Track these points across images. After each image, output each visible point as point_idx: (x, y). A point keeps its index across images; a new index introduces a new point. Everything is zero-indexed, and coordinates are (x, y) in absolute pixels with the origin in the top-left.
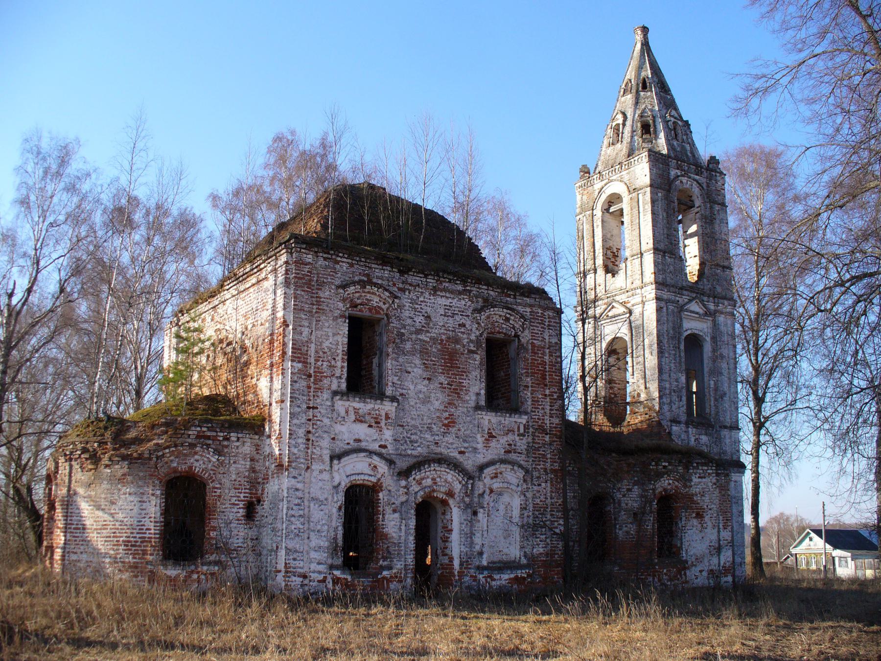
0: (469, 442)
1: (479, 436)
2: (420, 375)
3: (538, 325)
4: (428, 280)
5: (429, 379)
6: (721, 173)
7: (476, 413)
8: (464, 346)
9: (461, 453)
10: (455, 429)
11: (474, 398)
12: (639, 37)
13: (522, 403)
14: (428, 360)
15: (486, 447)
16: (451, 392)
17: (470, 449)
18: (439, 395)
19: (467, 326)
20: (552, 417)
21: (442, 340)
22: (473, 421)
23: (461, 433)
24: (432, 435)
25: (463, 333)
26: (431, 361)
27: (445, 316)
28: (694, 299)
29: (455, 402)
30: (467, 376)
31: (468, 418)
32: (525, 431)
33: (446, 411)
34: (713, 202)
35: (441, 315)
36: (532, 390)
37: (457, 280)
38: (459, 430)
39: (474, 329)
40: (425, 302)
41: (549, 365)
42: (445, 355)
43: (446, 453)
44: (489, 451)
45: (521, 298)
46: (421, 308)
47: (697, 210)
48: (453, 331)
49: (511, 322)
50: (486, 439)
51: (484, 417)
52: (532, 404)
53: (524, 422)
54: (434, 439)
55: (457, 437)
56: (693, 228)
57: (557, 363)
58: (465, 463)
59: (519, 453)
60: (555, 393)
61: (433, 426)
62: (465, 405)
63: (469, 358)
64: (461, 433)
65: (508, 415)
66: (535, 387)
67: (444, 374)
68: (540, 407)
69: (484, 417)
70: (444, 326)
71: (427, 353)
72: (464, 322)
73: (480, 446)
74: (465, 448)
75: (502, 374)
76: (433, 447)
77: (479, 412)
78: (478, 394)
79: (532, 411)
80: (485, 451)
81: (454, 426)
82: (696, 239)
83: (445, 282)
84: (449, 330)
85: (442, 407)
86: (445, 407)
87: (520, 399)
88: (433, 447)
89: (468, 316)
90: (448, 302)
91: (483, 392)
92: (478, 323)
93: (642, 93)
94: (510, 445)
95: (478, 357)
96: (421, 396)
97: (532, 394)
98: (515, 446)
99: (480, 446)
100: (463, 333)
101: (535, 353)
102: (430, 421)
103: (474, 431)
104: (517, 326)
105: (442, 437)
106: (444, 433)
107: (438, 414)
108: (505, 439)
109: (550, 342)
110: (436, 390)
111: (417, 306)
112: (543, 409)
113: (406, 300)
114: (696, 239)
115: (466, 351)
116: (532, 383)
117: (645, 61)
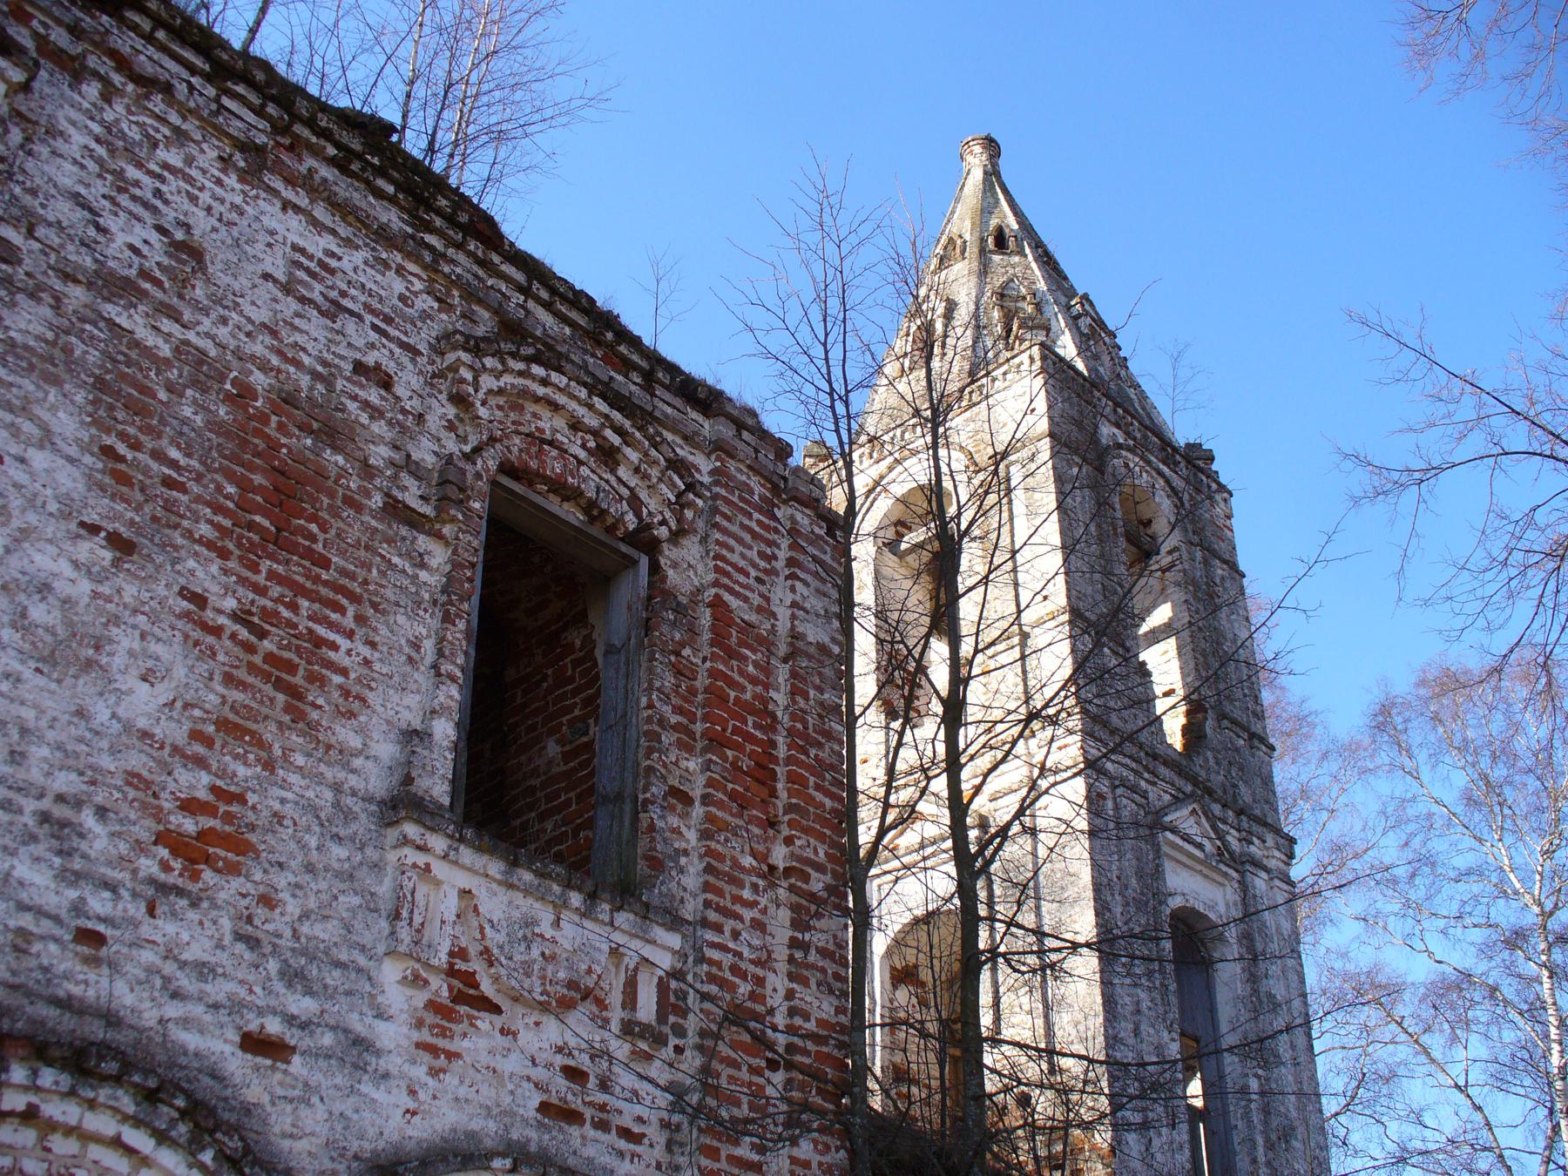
0: (327, 993)
1: (391, 973)
2: (65, 500)
3: (747, 538)
4: (226, 101)
5: (122, 546)
6: (1222, 488)
7: (392, 834)
8: (368, 471)
9: (255, 1043)
10: (237, 883)
11: (387, 750)
12: (976, 162)
13: (656, 864)
14: (136, 446)
15: (433, 1050)
16: (252, 668)
17: (327, 1039)
18: (168, 652)
19: (400, 390)
20: (805, 982)
21: (245, 393)
22: (367, 879)
23: (277, 923)
24: (76, 878)
25: (376, 413)
26: (158, 455)
27: (287, 289)
28: (1189, 797)
29: (269, 732)
30: (360, 619)
31: (339, 851)
32: (662, 1016)
33: (200, 763)
34: (1211, 552)
35: (267, 276)
36: (710, 818)
37: (381, 172)
38: (267, 901)
39: (433, 422)
40: (190, 180)
41: (791, 732)
42: (251, 467)
43: (150, 1017)
44: (450, 1079)
45: (678, 402)
46: (158, 193)
47: (1166, 560)
48: (316, 376)
49: (622, 472)
50: (432, 1006)
51: (440, 869)
52: (707, 887)
53: (665, 961)
54: (78, 908)
55: (253, 943)
56: (1162, 614)
57: (840, 676)
58: (280, 1120)
59: (625, 1133)
60: (820, 868)
61: (88, 819)
62: (330, 773)
63: (390, 541)
64: (277, 923)
65: (576, 899)
66: (720, 805)
67: (224, 554)
68: (748, 914)
69: (440, 869)
70: (274, 333)
71: (141, 411)
72: (390, 367)
73: (393, 1035)
74: (290, 1020)
75: (553, 749)
76: (58, 956)
77: (411, 830)
78: (413, 737)
79: (705, 923)
80: (420, 1072)
81: (233, 870)
82: (1171, 644)
83: (317, 152)
84: (298, 364)
85: (176, 732)
86: (196, 735)
87: (643, 843)
88: (58, 956)
89: (413, 351)
90: (318, 244)
91: (445, 730)
92: (460, 400)
93: (996, 258)
94: (574, 1075)
95: (439, 556)
96: (39, 613)
97: (705, 835)
98: (604, 1086)
99: (393, 1035)
100: (376, 413)
101: (731, 654)
102: (65, 782)
103: (367, 938)
104: (652, 504)
105: (137, 910)
106: (164, 889)
107: (137, 760)
108: (552, 1031)
109: (795, 636)
110: (154, 618)
111: (132, 173)
112: (758, 926)
113: (74, 115)
114: (1171, 644)
115: (377, 501)
116: (710, 783)
117: (997, 201)
